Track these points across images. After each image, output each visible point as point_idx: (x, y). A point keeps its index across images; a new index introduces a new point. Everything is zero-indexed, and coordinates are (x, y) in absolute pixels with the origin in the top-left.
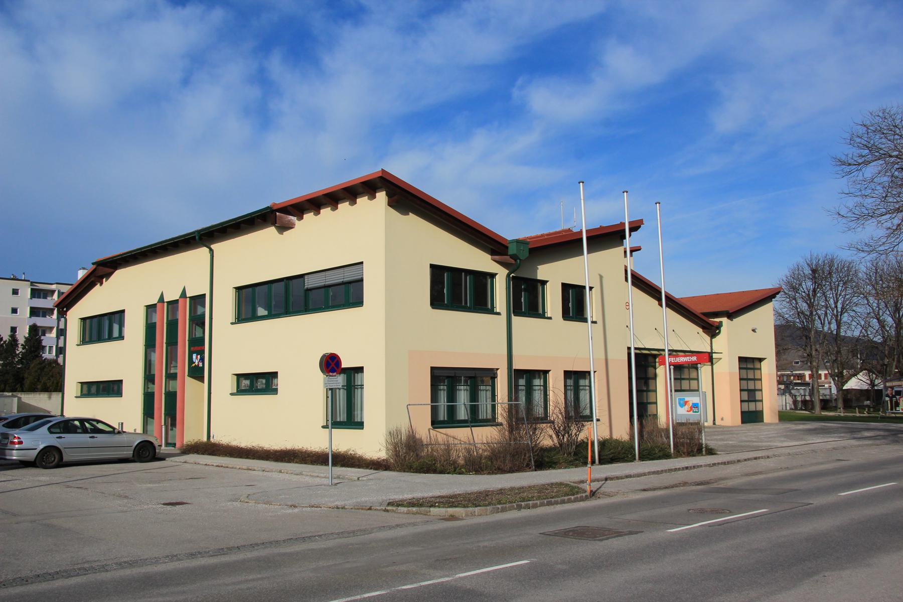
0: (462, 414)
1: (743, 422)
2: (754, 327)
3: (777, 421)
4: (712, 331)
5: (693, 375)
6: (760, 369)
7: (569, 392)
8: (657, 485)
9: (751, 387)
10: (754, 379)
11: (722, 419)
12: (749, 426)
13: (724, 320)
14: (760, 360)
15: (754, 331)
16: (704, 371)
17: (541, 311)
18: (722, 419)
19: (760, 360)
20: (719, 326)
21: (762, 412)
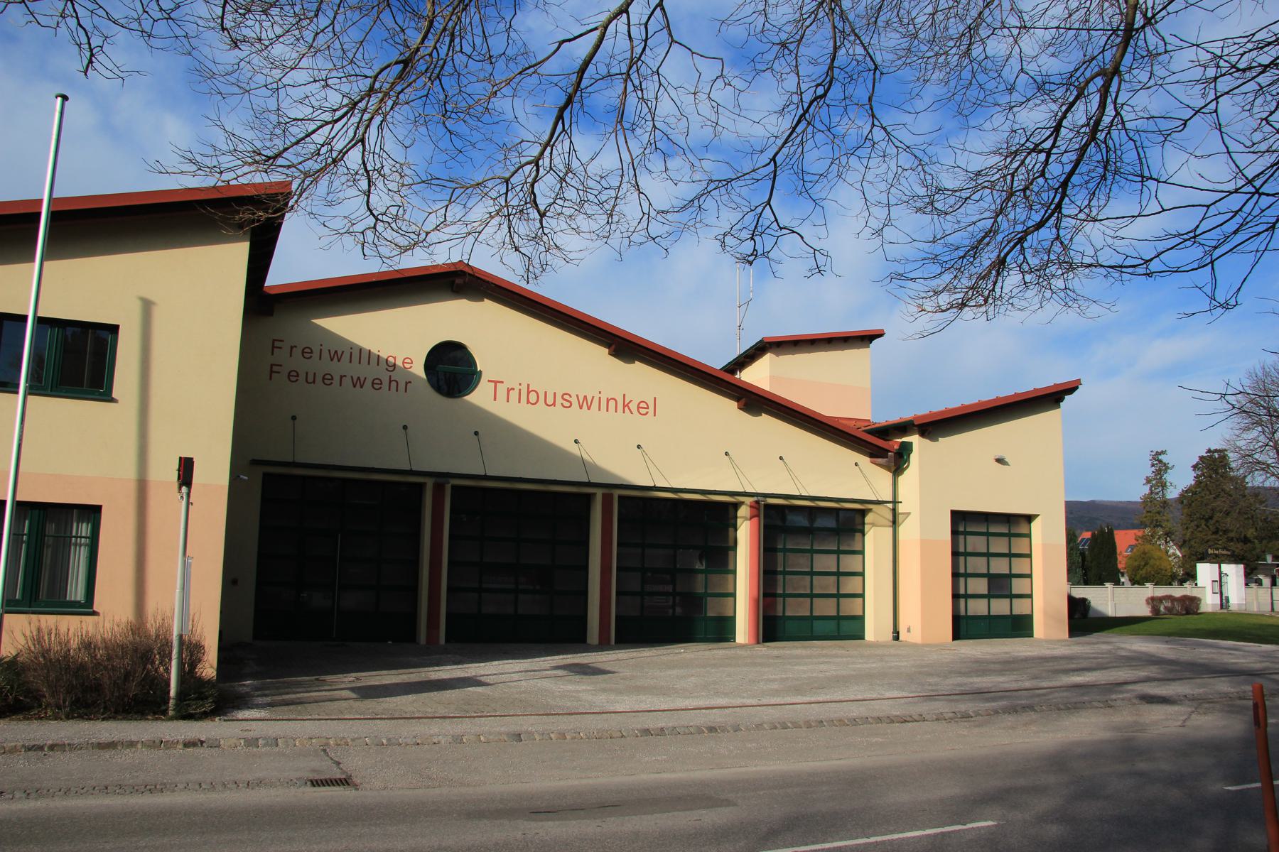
0: (1105, 599)
1: (956, 636)
2: (999, 454)
3: (1064, 633)
4: (898, 461)
5: (1024, 531)
6: (1029, 536)
7: (968, 529)
8: (565, 718)
9: (999, 566)
10: (1010, 555)
11: (909, 630)
12: (956, 642)
13: (915, 439)
14: (1029, 518)
15: (1000, 461)
16: (875, 539)
17: (76, 592)
18: (909, 630)
19: (1029, 518)
20: (906, 450)
21: (861, 619)
